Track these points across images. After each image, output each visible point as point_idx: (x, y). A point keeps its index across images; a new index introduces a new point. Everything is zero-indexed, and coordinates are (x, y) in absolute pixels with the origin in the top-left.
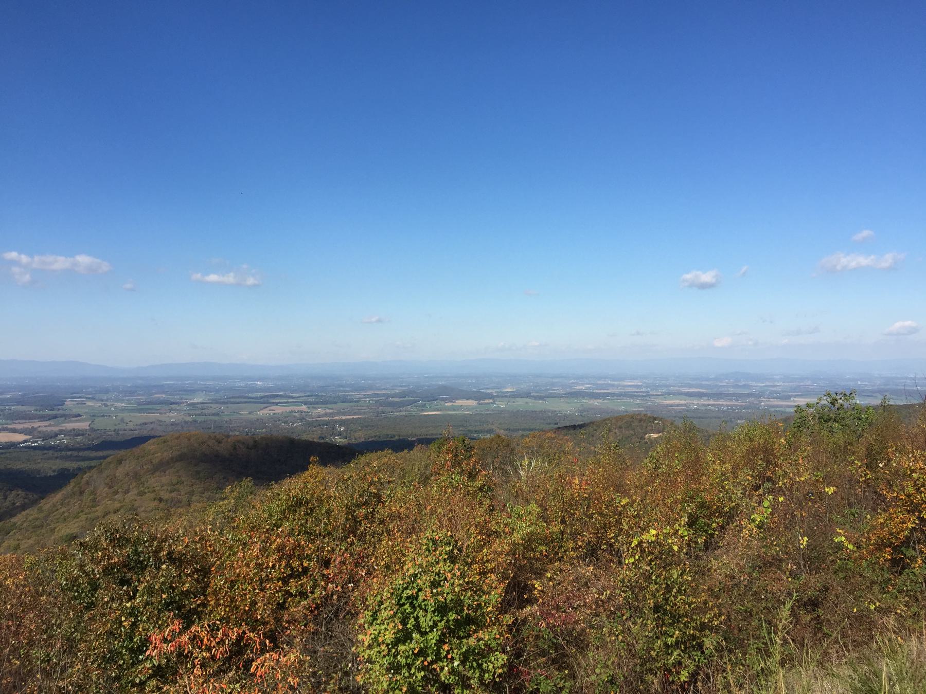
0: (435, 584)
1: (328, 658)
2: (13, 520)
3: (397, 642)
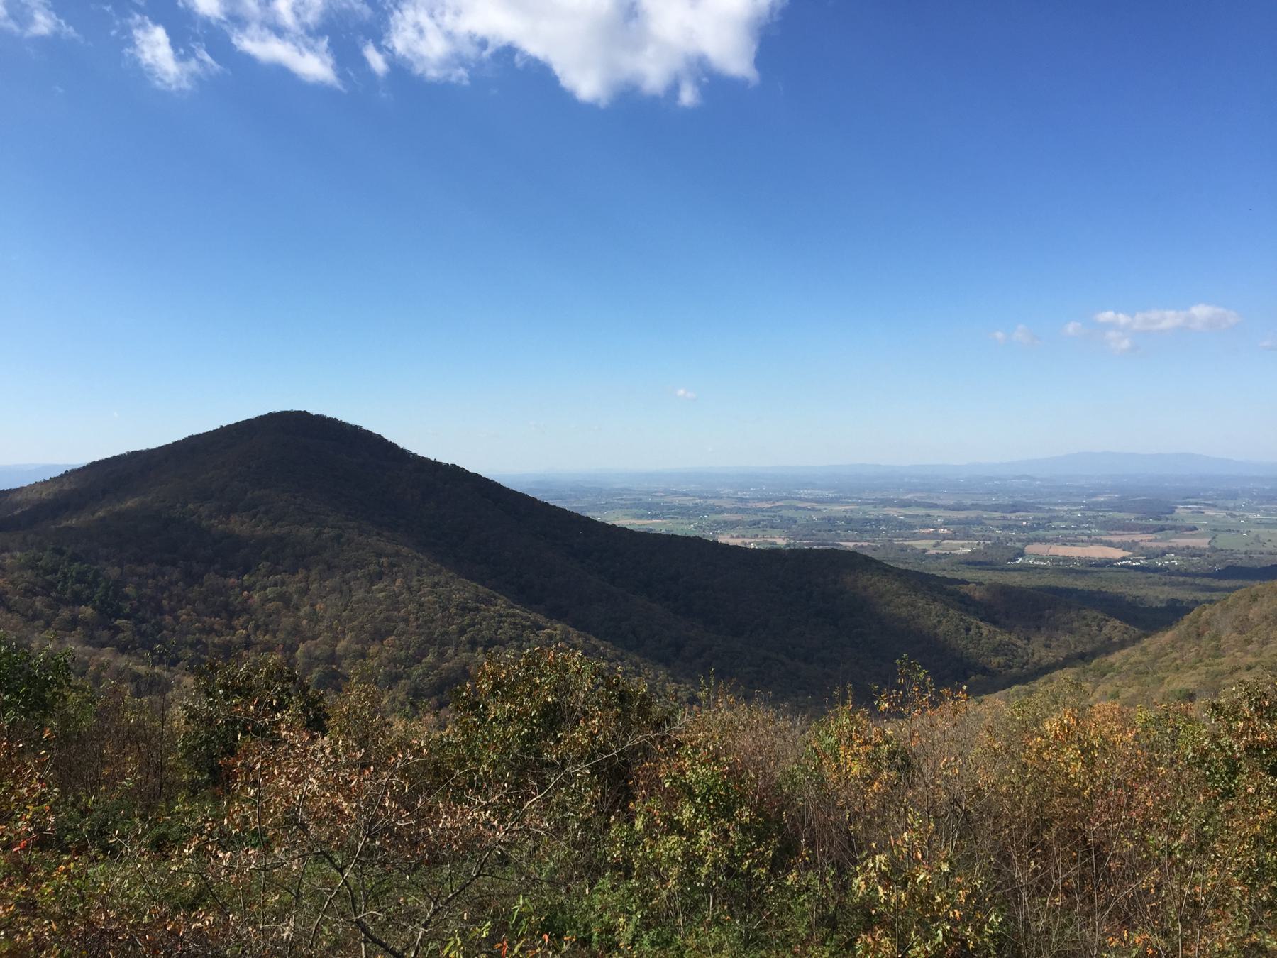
2: (1111, 659)
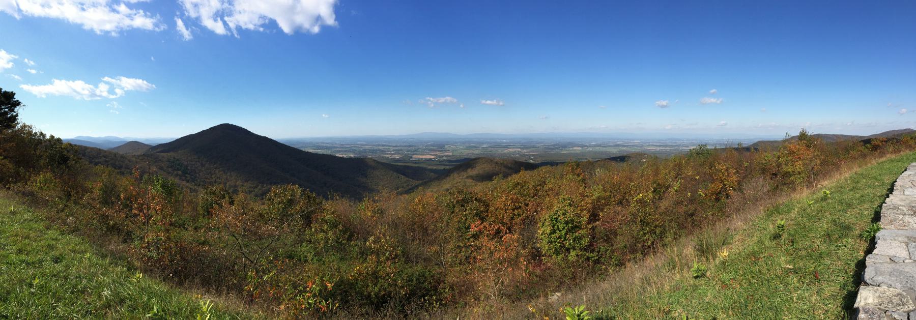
0: (564, 214)
1: (528, 237)
3: (551, 234)
